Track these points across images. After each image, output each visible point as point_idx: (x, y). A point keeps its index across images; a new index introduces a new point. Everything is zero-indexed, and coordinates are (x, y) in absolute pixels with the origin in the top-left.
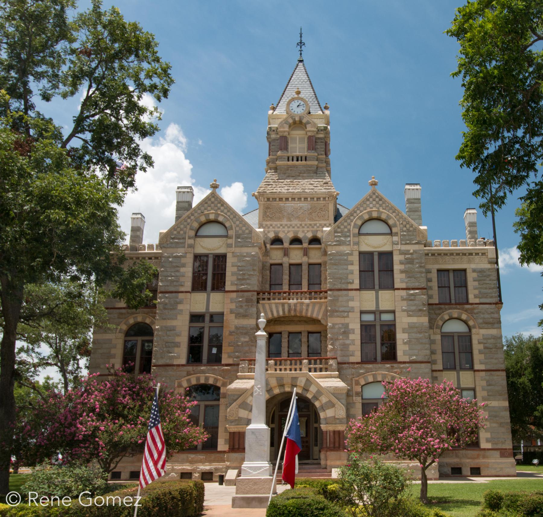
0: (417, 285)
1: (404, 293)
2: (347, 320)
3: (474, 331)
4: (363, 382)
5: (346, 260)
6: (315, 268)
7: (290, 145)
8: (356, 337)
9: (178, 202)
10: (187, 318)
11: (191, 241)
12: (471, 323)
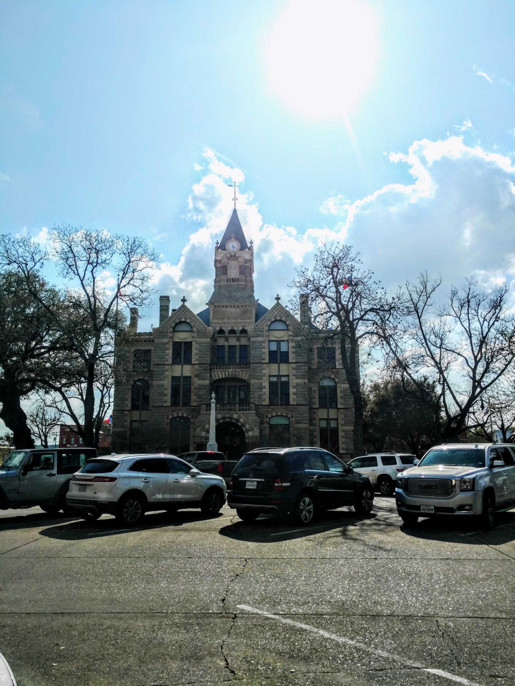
0: (302, 360)
1: (294, 365)
2: (261, 381)
3: (338, 385)
4: (270, 416)
5: (261, 345)
6: (245, 349)
7: (229, 271)
8: (267, 390)
9: (161, 306)
10: (170, 379)
11: (171, 335)
12: (337, 380)
